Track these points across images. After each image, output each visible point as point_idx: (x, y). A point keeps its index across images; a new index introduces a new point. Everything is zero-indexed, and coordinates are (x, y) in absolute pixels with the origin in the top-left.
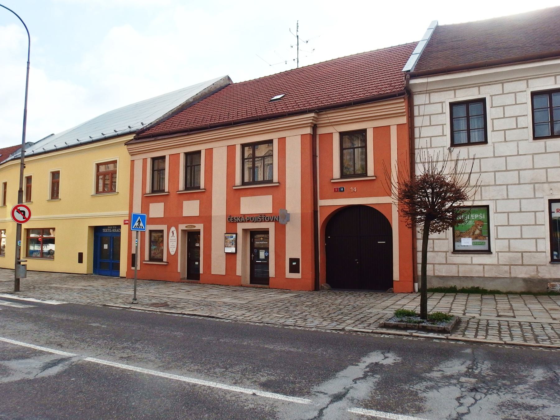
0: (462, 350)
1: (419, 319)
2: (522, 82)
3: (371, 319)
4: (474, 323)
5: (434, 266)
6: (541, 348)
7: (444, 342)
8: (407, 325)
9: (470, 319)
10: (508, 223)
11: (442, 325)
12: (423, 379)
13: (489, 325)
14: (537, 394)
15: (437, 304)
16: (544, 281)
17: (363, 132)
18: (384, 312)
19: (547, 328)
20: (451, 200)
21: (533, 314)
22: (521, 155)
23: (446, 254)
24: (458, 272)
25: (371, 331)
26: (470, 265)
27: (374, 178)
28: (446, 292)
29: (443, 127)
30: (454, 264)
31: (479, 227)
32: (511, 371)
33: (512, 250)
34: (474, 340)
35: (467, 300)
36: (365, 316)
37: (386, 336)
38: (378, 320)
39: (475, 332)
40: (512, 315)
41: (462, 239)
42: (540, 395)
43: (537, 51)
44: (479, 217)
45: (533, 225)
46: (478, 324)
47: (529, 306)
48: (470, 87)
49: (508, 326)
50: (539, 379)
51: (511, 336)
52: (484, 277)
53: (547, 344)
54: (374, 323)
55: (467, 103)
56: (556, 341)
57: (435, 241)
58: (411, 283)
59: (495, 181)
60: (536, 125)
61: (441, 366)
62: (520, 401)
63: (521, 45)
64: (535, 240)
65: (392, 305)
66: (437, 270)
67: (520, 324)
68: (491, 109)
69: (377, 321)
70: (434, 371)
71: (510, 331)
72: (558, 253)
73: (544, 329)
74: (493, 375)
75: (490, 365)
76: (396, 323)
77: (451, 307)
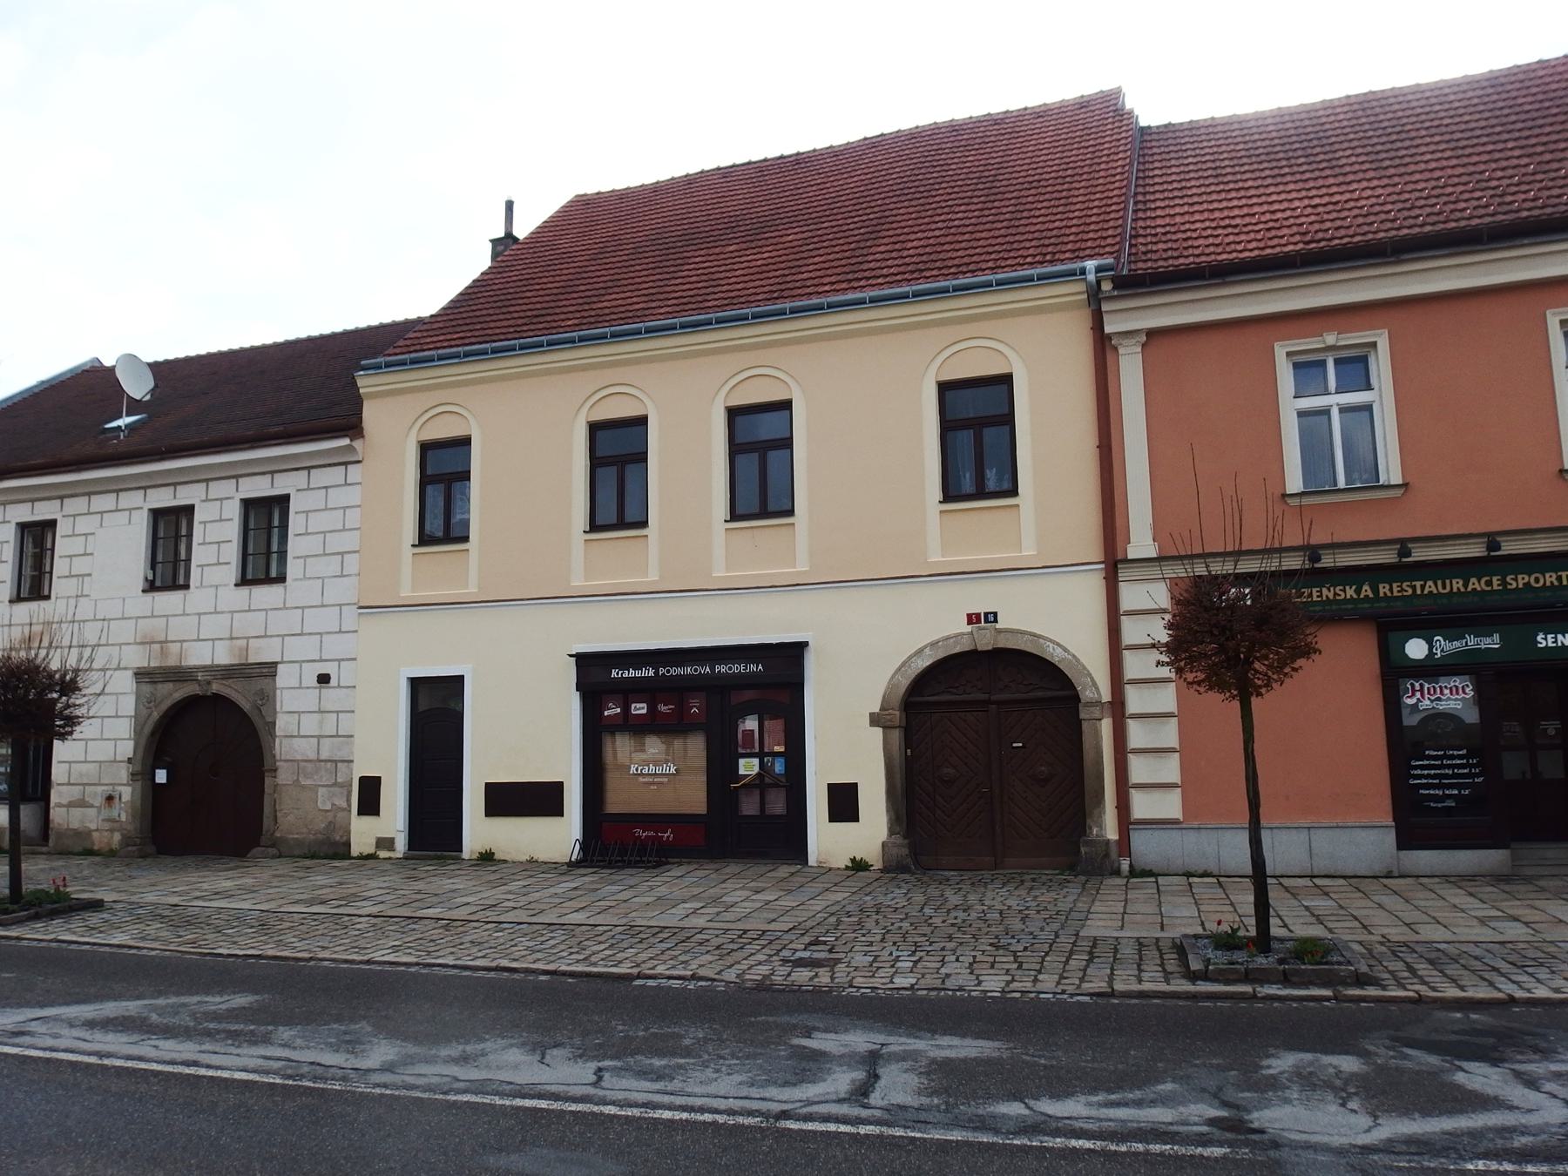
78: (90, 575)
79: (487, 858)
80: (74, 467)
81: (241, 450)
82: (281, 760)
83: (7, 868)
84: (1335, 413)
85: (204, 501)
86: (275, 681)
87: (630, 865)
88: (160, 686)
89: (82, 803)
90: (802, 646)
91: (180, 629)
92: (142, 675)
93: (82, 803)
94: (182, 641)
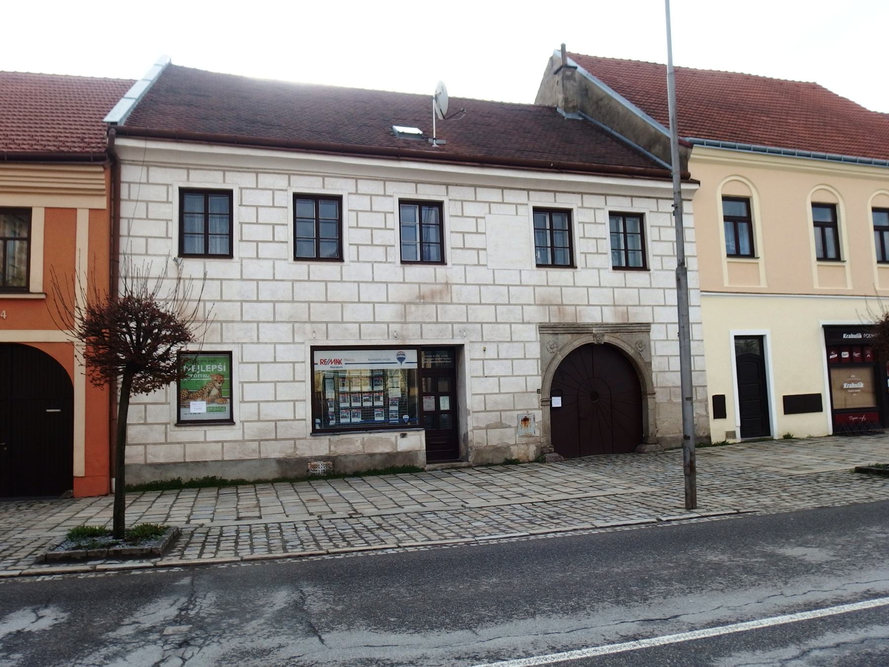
0: (176, 582)
1: (111, 539)
2: (282, 176)
3: (22, 550)
4: (201, 535)
5: (145, 447)
6: (289, 559)
7: (149, 572)
8: (87, 553)
9: (196, 528)
10: (259, 379)
11: (147, 546)
12: (102, 644)
13: (223, 535)
14: (274, 630)
15: (147, 510)
16: (303, 461)
17: (23, 215)
18: (51, 534)
19: (301, 529)
20: (168, 342)
21: (286, 510)
22: (277, 280)
23: (166, 428)
24: (184, 455)
25: (17, 573)
26: (203, 442)
27: (43, 296)
28: (164, 490)
29: (167, 224)
30: (179, 443)
31: (217, 385)
32: (243, 602)
33: (262, 417)
34: (196, 561)
35: (196, 498)
36: (11, 546)
37: (47, 578)
38: (35, 550)
39: (200, 548)
40: (257, 514)
41: (192, 403)
42: (278, 630)
43: (304, 138)
44: (217, 368)
45: (291, 382)
46: (207, 535)
47: (282, 499)
48: (210, 170)
49: (250, 532)
50: (280, 606)
51: (252, 547)
52: (223, 461)
53: (298, 551)
54: (26, 557)
55: (207, 193)
56: (309, 546)
57: (148, 406)
58: (105, 480)
59: (242, 315)
60: (298, 241)
61: (137, 614)
62: (248, 645)
63: (284, 125)
64: (292, 403)
65: (68, 519)
66: (151, 455)
67: (266, 528)
68: (240, 207)
69: (33, 552)
70: (123, 625)
71: (251, 540)
72: (321, 421)
73: (296, 530)
74: (218, 613)
75: (214, 598)
76: (67, 552)
77: (169, 513)
78: (485, 249)
79: (788, 437)
80: (304, 150)
81: (543, 172)
82: (657, 387)
85: (580, 208)
86: (649, 335)
87: (862, 434)
88: (560, 337)
89: (500, 425)
91: (571, 296)
92: (544, 328)
93: (500, 425)
94: (576, 305)
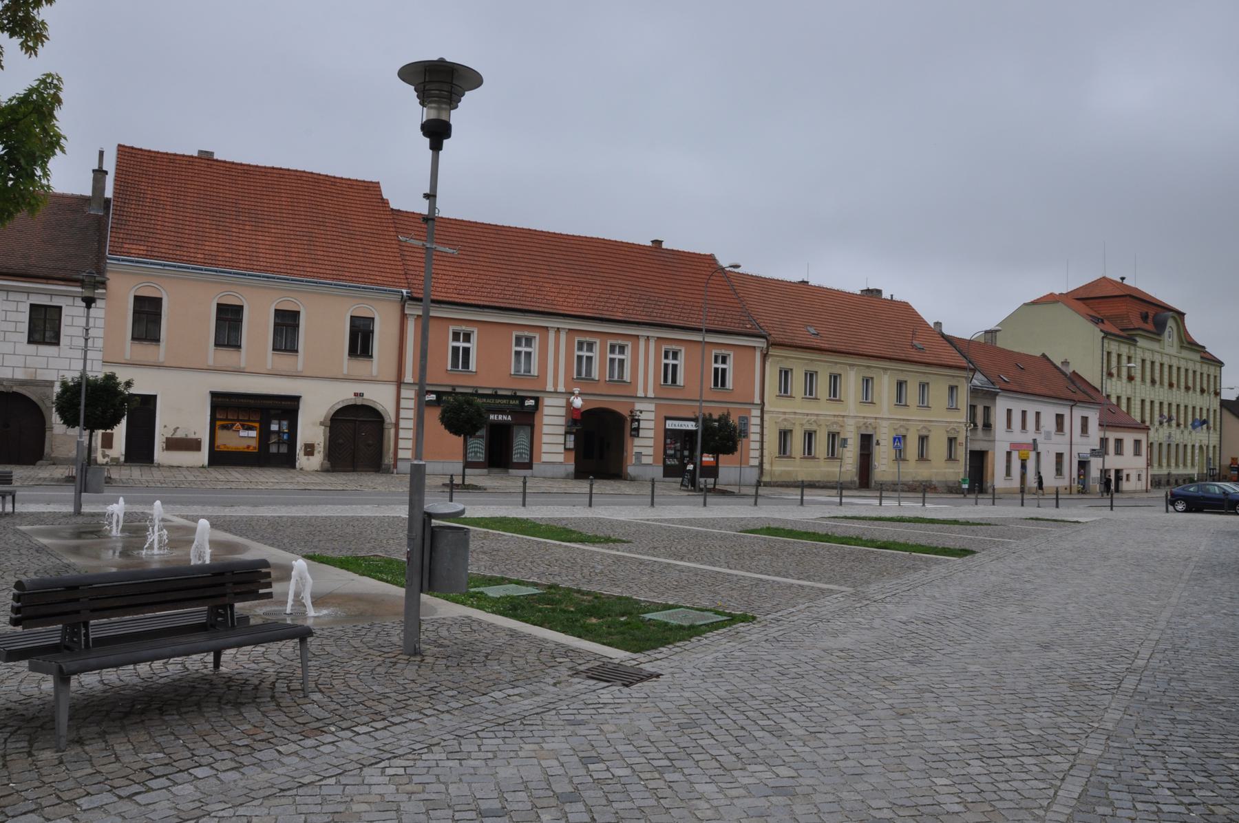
79: (301, 469)
83: (426, 481)
84: (585, 359)
90: (300, 397)
